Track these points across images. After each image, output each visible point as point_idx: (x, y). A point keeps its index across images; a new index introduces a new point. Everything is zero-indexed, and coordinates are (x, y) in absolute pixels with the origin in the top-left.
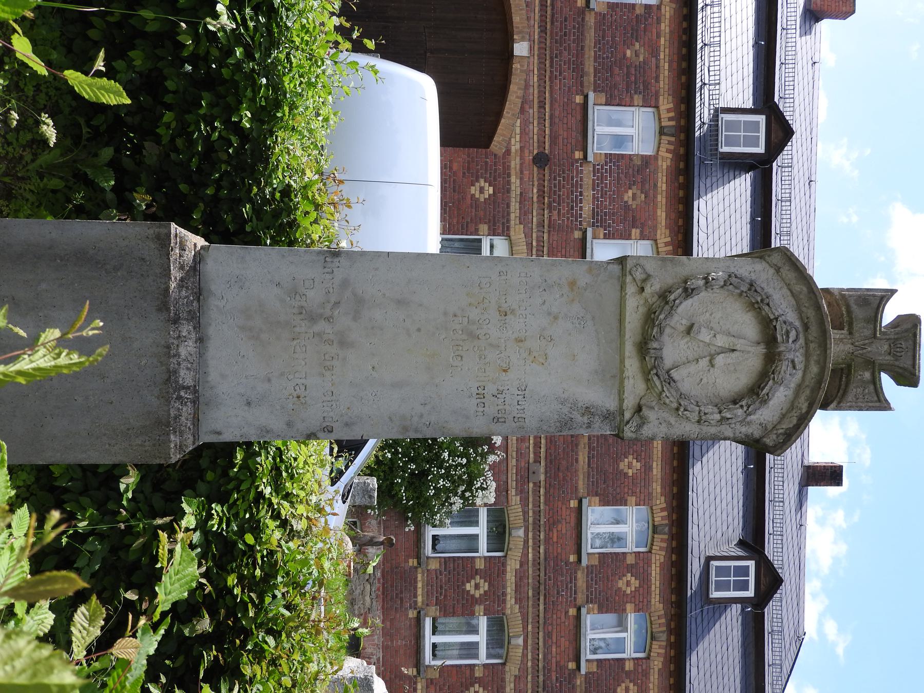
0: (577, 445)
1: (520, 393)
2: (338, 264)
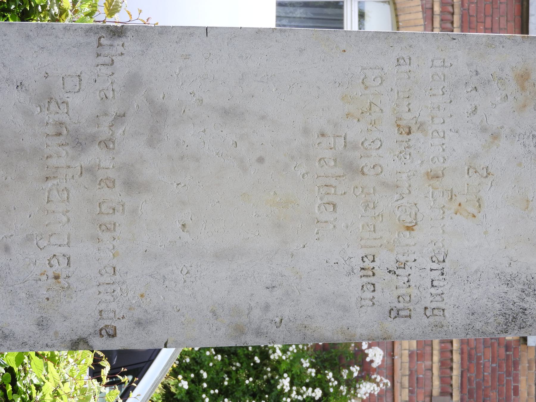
0: (516, 364)
1: (435, 266)
2: (120, 49)
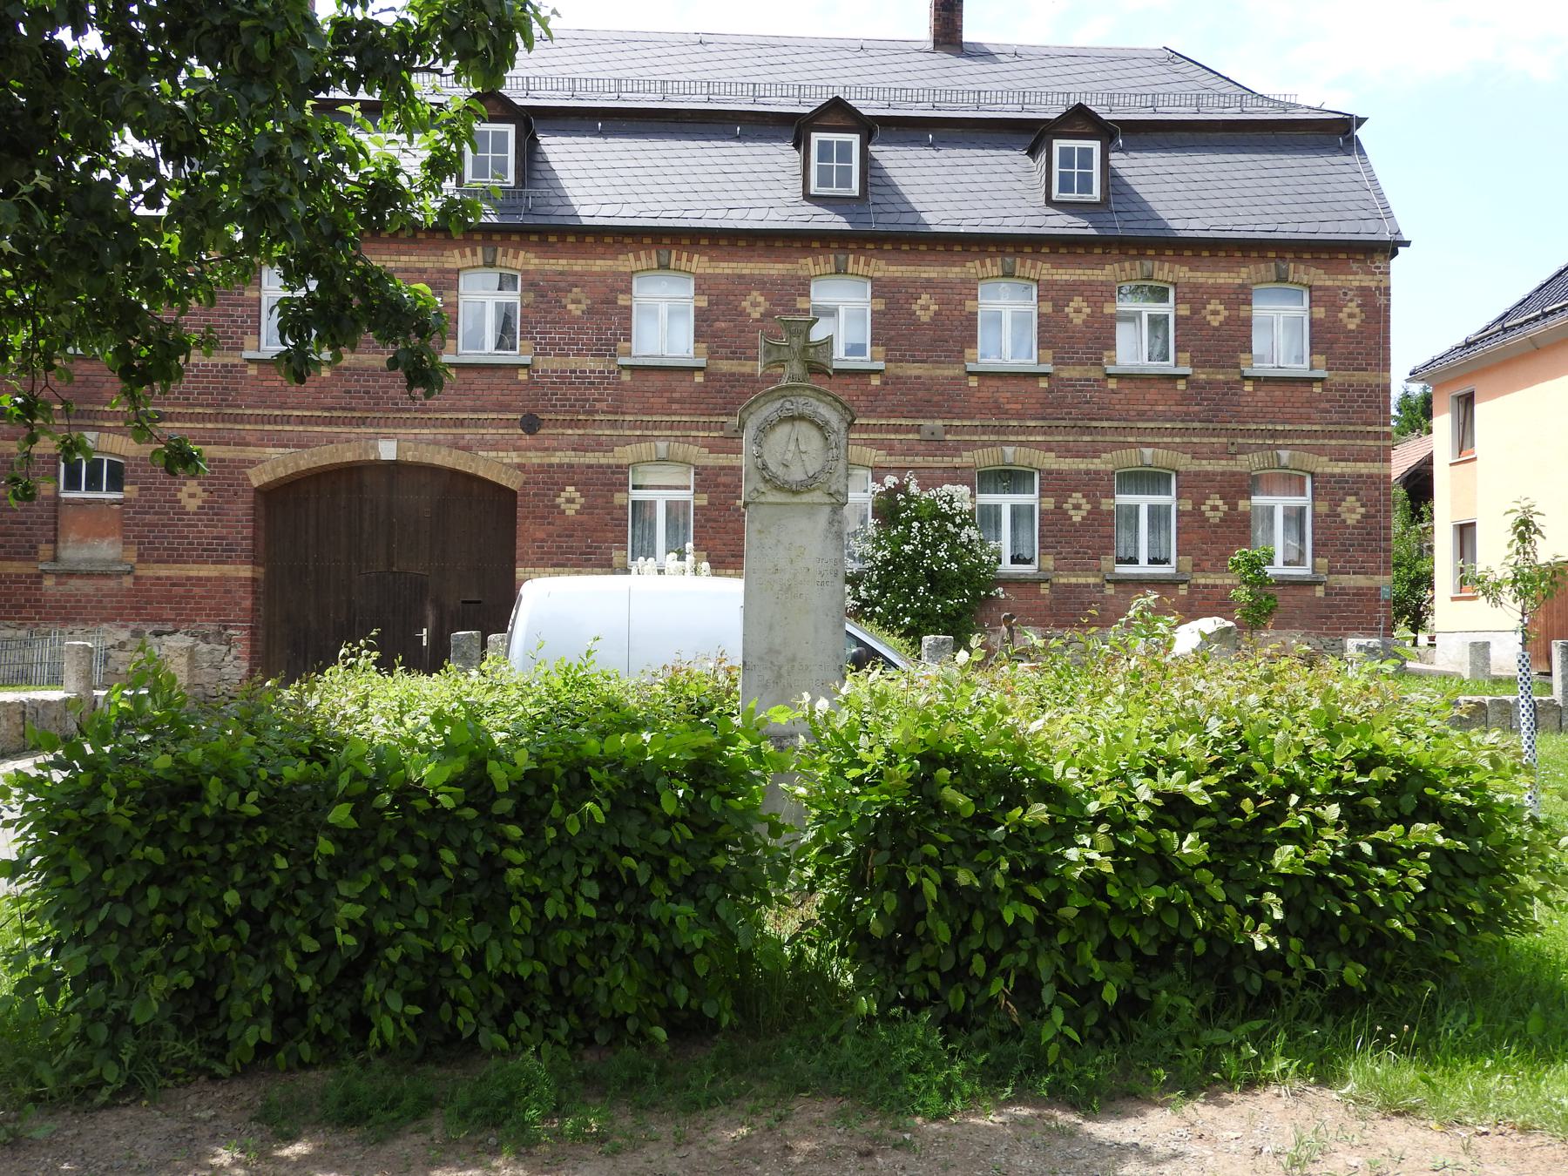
0: (898, 378)
